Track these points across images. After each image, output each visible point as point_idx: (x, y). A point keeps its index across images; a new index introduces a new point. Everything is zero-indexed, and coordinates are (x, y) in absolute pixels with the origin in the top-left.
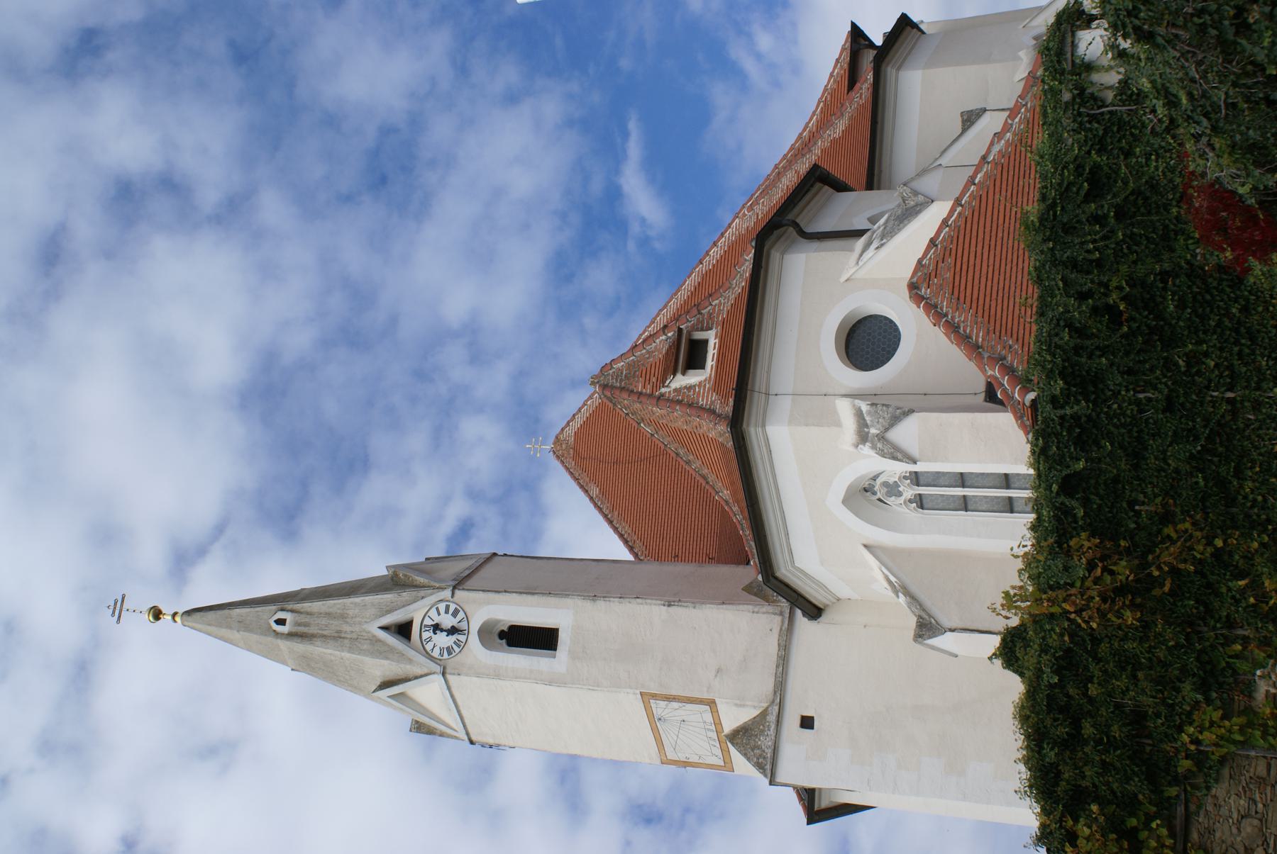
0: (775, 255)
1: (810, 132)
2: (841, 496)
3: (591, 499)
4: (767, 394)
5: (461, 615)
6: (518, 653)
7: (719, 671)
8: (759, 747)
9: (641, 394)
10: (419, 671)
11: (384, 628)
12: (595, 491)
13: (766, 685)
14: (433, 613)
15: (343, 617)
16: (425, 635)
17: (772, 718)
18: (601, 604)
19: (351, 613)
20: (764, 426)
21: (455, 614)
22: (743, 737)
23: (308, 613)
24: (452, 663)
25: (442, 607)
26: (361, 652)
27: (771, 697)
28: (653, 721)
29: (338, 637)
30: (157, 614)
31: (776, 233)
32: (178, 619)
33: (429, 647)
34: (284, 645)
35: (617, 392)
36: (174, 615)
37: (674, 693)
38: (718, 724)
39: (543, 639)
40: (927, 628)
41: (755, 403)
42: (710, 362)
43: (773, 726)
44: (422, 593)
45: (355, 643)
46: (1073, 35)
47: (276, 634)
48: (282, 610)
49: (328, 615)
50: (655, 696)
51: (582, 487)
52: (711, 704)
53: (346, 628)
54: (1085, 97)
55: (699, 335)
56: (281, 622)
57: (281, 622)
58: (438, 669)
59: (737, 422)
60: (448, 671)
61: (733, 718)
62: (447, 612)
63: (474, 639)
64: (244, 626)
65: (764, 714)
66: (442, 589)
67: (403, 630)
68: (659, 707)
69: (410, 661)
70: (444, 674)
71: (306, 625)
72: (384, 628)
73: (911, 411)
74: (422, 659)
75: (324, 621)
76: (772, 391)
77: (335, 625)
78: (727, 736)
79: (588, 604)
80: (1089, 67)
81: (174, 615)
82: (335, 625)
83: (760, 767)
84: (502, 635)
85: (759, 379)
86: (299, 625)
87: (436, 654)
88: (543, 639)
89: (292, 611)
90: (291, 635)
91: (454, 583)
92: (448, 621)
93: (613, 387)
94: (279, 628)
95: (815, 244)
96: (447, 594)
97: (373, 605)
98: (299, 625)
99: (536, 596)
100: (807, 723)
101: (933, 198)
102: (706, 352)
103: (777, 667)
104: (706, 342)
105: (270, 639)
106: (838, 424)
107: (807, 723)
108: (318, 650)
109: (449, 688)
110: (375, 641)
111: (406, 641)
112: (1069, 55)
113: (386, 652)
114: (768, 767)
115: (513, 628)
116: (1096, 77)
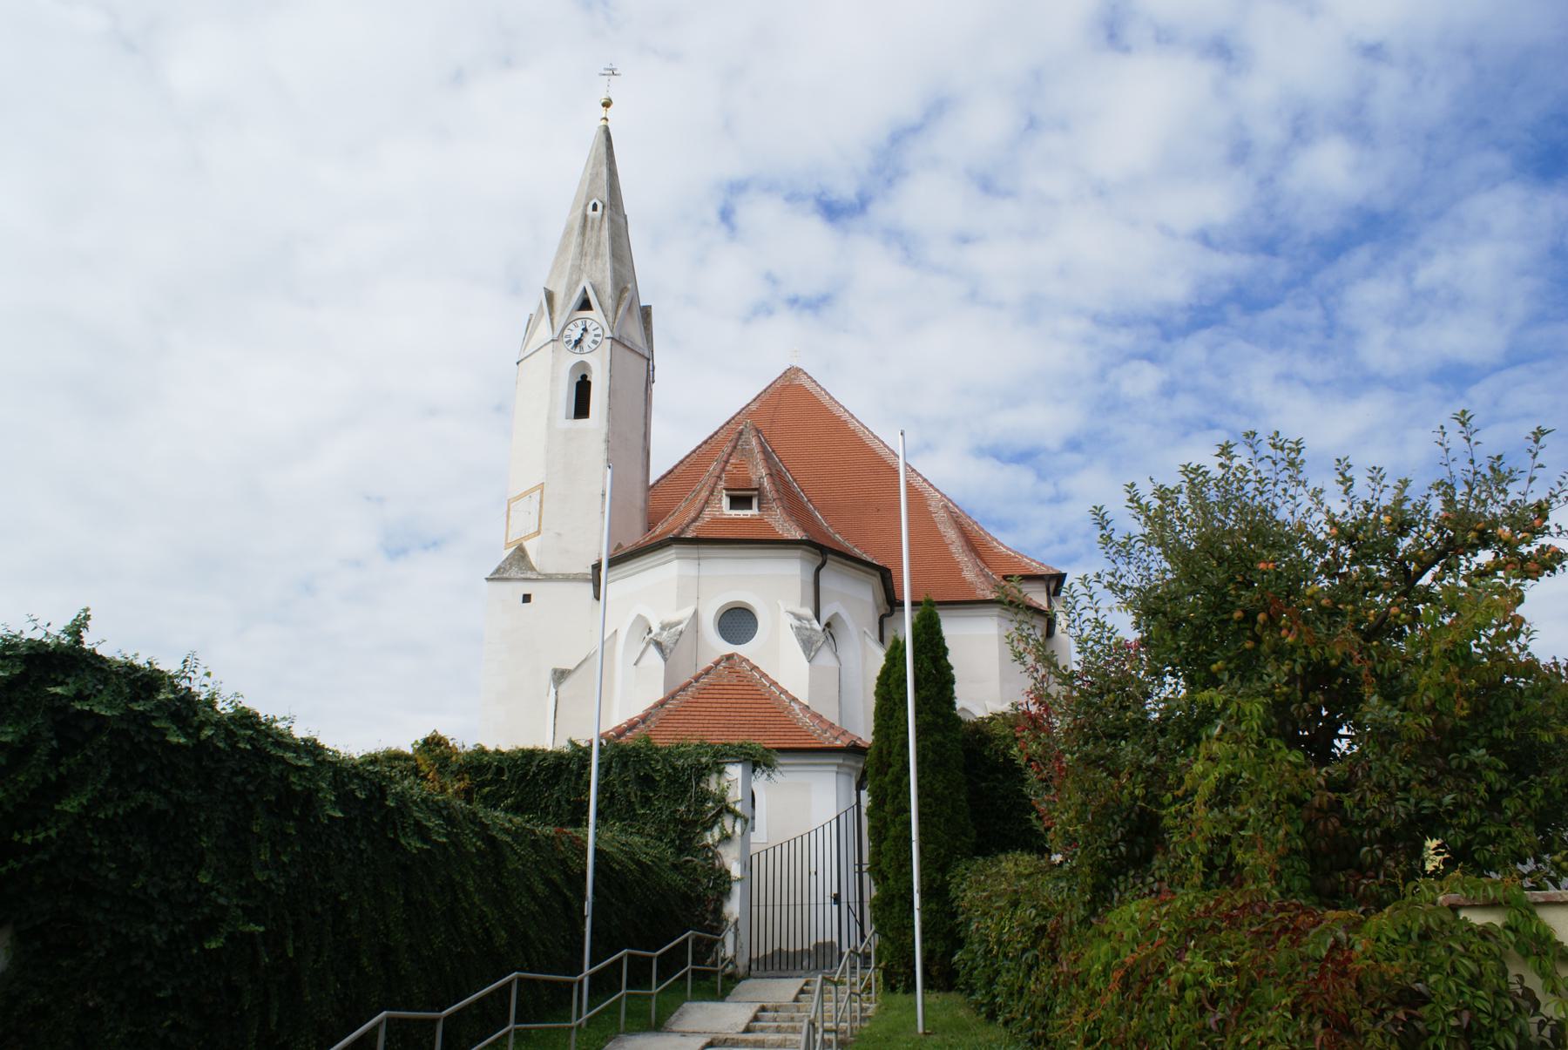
0: (799, 553)
1: (995, 547)
2: (642, 614)
3: (749, 405)
4: (699, 558)
5: (594, 346)
6: (569, 392)
7: (559, 534)
8: (511, 568)
9: (727, 462)
10: (555, 321)
11: (585, 291)
12: (753, 407)
13: (550, 570)
14: (595, 325)
15: (597, 255)
16: (579, 322)
17: (529, 575)
18: (603, 446)
19: (599, 261)
20: (678, 558)
21: (595, 342)
22: (520, 555)
23: (600, 228)
24: (561, 345)
25: (599, 331)
26: (571, 274)
27: (543, 572)
28: (532, 491)
29: (582, 254)
30: (607, 104)
31: (818, 551)
32: (603, 122)
33: (571, 326)
34: (579, 213)
35: (732, 444)
36: (606, 119)
37: (544, 506)
38: (528, 537)
39: (581, 408)
40: (560, 676)
41: (692, 551)
42: (734, 513)
43: (523, 576)
44: (610, 314)
45: (578, 269)
46: (740, 762)
47: (587, 205)
48: (604, 207)
49: (599, 244)
50: (542, 492)
51: (759, 396)
52: (539, 532)
53: (589, 258)
54: (701, 772)
55: (755, 502)
56: (595, 208)
57: (595, 208)
58: (556, 336)
59: (678, 540)
60: (555, 343)
61: (531, 548)
62: (596, 336)
63: (577, 358)
64: (594, 177)
65: (532, 569)
66: (612, 331)
67: (585, 305)
68: (536, 495)
69: (562, 314)
70: (553, 340)
71: (592, 228)
72: (585, 291)
73: (665, 660)
74: (562, 324)
75: (594, 241)
76: (702, 562)
77: (590, 250)
78: (521, 544)
79: (603, 437)
80: (721, 772)
81: (606, 119)
82: (590, 250)
83: (497, 571)
84: (584, 377)
85: (706, 551)
86: (593, 222)
87: (567, 332)
88: (581, 408)
89: (603, 215)
90: (585, 217)
91: (617, 337)
92: (588, 339)
93: (738, 439)
94: (590, 207)
95: (810, 579)
96: (608, 334)
97: (604, 278)
98: (593, 222)
99: (607, 399)
100: (527, 598)
101: (813, 663)
102: (743, 509)
103: (563, 575)
104: (751, 508)
105: (583, 202)
106: (678, 609)
107: (527, 598)
108: (575, 239)
109: (546, 345)
110: (577, 283)
111: (578, 306)
112: (726, 760)
113: (569, 294)
114: (497, 576)
115: (589, 383)
116: (715, 776)
